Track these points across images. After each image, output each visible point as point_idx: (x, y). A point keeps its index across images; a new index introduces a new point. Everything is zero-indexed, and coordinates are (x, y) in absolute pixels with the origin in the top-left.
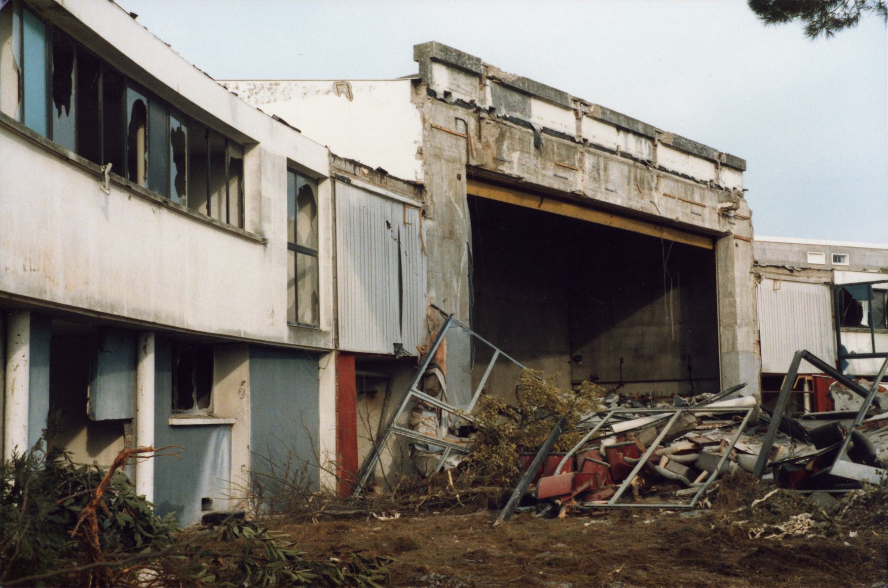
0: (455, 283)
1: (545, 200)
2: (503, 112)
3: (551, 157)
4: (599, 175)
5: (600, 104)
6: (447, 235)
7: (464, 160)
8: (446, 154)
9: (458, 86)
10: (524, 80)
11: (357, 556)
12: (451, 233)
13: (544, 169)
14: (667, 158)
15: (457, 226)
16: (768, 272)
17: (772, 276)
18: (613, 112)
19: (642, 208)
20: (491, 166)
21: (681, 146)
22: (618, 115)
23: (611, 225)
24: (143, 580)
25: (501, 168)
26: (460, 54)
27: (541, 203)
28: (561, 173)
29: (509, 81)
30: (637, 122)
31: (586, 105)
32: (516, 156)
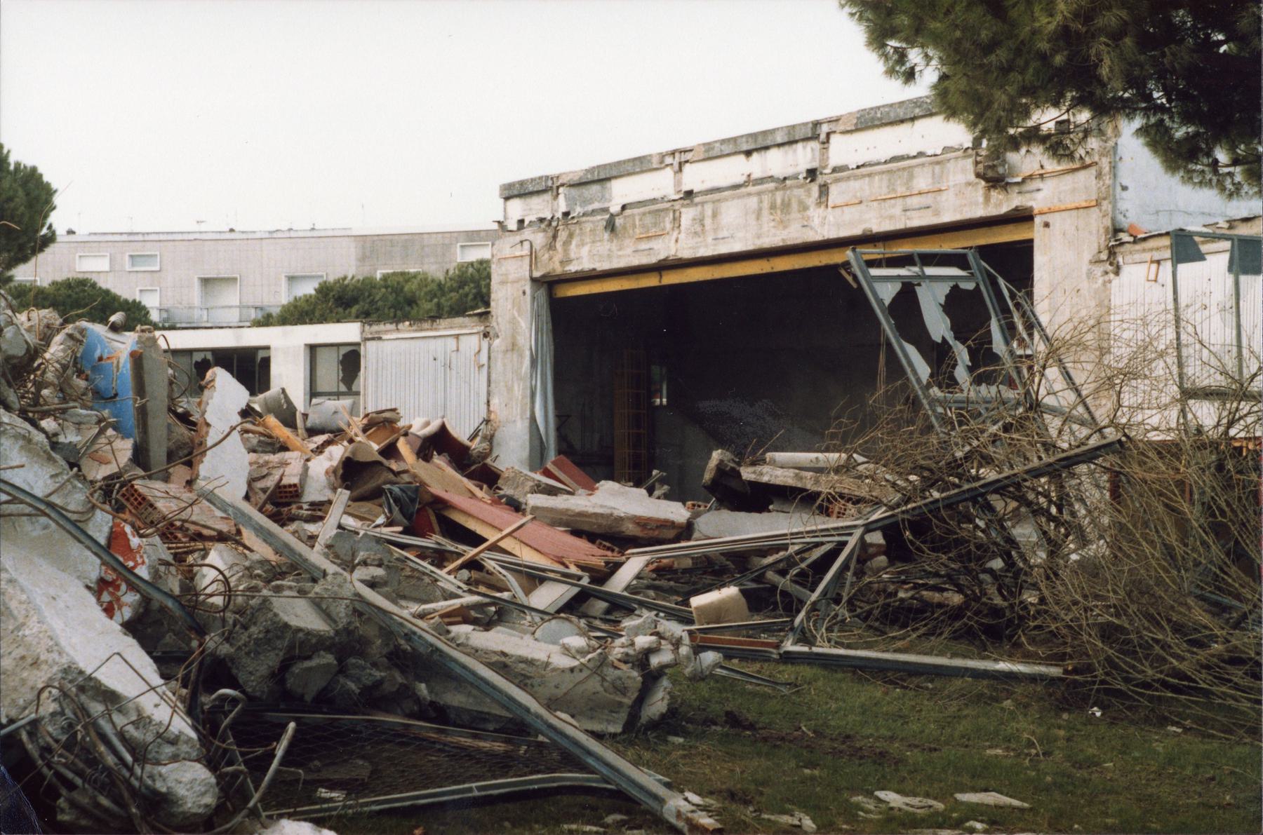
0: (516, 388)
1: (664, 273)
2: (578, 210)
3: (631, 232)
4: (704, 226)
5: (701, 142)
6: (510, 348)
7: (527, 274)
8: (511, 277)
9: (531, 209)
10: (592, 170)
11: (567, 567)
12: (514, 345)
13: (620, 250)
14: (844, 150)
15: (519, 338)
16: (1151, 250)
17: (1147, 256)
18: (723, 142)
19: (783, 240)
20: (559, 270)
21: (711, 153)
22: (734, 140)
23: (775, 270)
24: (1241, 407)
25: (567, 268)
26: (522, 183)
27: (661, 276)
28: (644, 246)
29: (576, 179)
30: (773, 131)
31: (691, 150)
32: (585, 251)
